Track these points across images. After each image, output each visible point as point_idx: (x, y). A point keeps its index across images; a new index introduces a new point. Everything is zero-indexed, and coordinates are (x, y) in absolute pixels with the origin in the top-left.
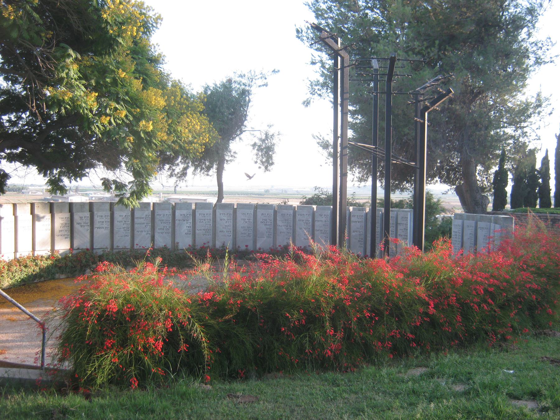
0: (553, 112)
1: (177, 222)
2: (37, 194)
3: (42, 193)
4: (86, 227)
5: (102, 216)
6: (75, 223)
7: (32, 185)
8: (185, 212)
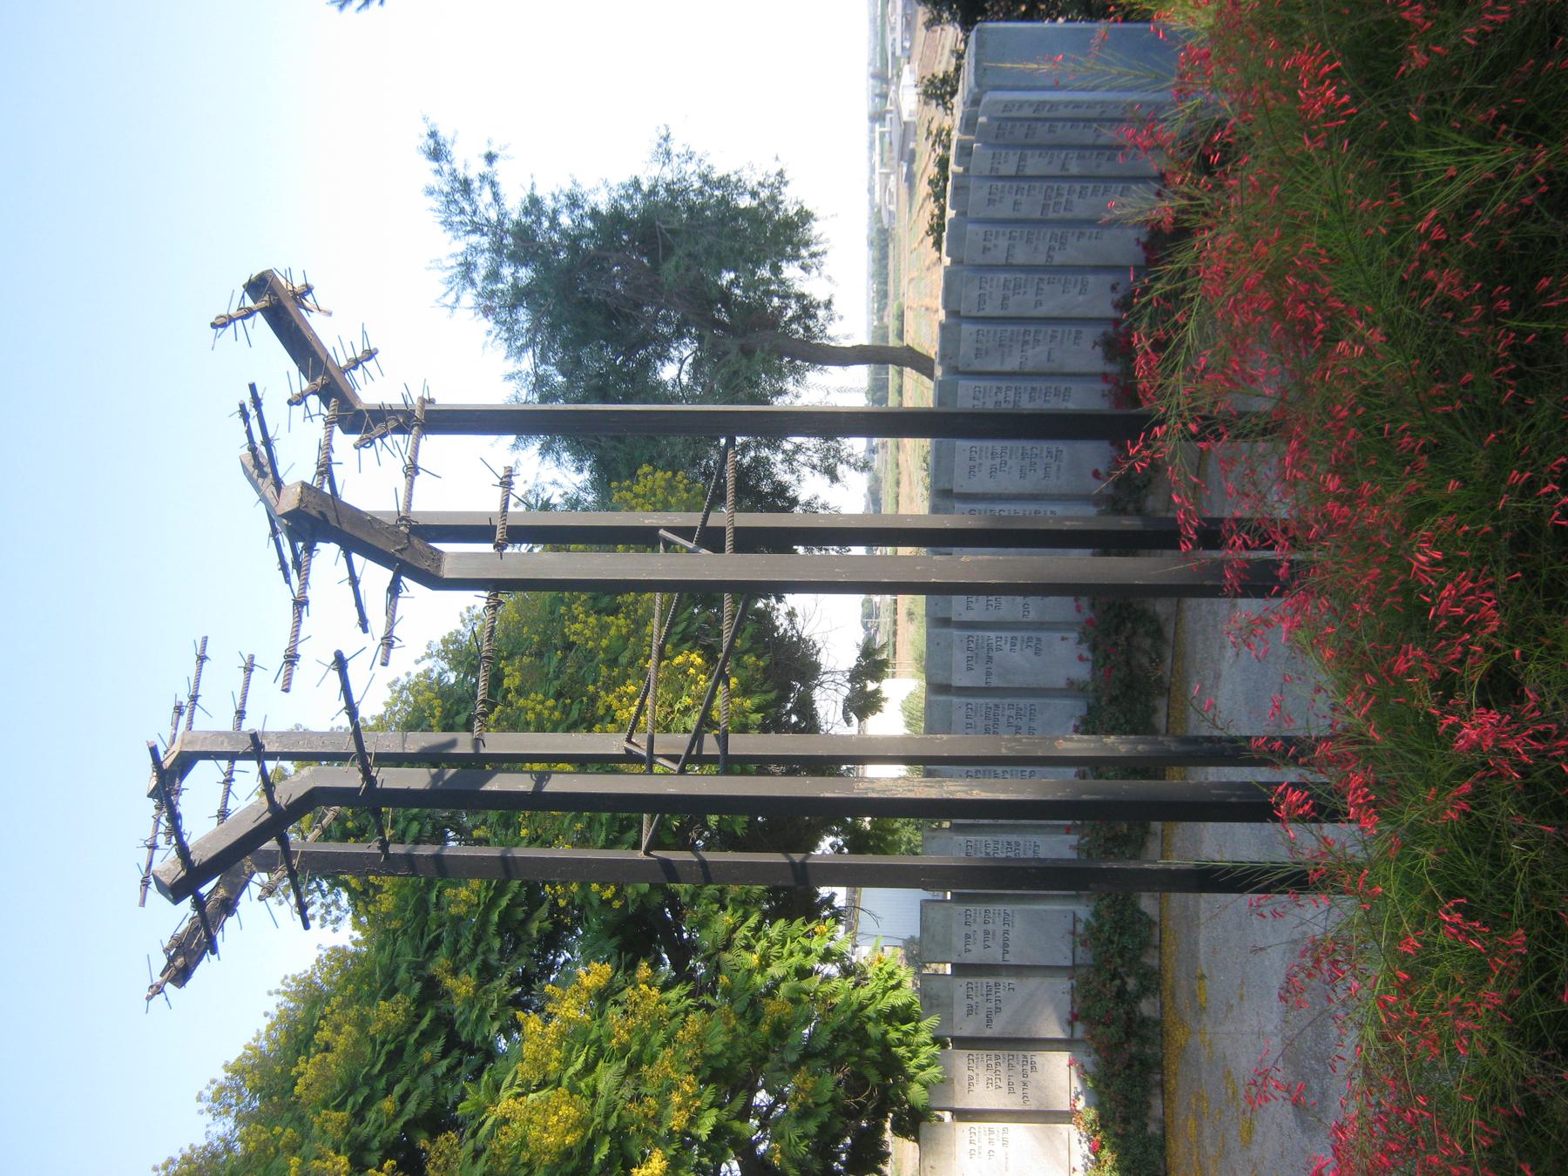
0: (300, 650)
1: (995, 682)
2: (894, 190)
3: (893, 177)
4: (1002, 993)
5: (967, 936)
6: (988, 1033)
7: (871, 190)
8: (959, 657)
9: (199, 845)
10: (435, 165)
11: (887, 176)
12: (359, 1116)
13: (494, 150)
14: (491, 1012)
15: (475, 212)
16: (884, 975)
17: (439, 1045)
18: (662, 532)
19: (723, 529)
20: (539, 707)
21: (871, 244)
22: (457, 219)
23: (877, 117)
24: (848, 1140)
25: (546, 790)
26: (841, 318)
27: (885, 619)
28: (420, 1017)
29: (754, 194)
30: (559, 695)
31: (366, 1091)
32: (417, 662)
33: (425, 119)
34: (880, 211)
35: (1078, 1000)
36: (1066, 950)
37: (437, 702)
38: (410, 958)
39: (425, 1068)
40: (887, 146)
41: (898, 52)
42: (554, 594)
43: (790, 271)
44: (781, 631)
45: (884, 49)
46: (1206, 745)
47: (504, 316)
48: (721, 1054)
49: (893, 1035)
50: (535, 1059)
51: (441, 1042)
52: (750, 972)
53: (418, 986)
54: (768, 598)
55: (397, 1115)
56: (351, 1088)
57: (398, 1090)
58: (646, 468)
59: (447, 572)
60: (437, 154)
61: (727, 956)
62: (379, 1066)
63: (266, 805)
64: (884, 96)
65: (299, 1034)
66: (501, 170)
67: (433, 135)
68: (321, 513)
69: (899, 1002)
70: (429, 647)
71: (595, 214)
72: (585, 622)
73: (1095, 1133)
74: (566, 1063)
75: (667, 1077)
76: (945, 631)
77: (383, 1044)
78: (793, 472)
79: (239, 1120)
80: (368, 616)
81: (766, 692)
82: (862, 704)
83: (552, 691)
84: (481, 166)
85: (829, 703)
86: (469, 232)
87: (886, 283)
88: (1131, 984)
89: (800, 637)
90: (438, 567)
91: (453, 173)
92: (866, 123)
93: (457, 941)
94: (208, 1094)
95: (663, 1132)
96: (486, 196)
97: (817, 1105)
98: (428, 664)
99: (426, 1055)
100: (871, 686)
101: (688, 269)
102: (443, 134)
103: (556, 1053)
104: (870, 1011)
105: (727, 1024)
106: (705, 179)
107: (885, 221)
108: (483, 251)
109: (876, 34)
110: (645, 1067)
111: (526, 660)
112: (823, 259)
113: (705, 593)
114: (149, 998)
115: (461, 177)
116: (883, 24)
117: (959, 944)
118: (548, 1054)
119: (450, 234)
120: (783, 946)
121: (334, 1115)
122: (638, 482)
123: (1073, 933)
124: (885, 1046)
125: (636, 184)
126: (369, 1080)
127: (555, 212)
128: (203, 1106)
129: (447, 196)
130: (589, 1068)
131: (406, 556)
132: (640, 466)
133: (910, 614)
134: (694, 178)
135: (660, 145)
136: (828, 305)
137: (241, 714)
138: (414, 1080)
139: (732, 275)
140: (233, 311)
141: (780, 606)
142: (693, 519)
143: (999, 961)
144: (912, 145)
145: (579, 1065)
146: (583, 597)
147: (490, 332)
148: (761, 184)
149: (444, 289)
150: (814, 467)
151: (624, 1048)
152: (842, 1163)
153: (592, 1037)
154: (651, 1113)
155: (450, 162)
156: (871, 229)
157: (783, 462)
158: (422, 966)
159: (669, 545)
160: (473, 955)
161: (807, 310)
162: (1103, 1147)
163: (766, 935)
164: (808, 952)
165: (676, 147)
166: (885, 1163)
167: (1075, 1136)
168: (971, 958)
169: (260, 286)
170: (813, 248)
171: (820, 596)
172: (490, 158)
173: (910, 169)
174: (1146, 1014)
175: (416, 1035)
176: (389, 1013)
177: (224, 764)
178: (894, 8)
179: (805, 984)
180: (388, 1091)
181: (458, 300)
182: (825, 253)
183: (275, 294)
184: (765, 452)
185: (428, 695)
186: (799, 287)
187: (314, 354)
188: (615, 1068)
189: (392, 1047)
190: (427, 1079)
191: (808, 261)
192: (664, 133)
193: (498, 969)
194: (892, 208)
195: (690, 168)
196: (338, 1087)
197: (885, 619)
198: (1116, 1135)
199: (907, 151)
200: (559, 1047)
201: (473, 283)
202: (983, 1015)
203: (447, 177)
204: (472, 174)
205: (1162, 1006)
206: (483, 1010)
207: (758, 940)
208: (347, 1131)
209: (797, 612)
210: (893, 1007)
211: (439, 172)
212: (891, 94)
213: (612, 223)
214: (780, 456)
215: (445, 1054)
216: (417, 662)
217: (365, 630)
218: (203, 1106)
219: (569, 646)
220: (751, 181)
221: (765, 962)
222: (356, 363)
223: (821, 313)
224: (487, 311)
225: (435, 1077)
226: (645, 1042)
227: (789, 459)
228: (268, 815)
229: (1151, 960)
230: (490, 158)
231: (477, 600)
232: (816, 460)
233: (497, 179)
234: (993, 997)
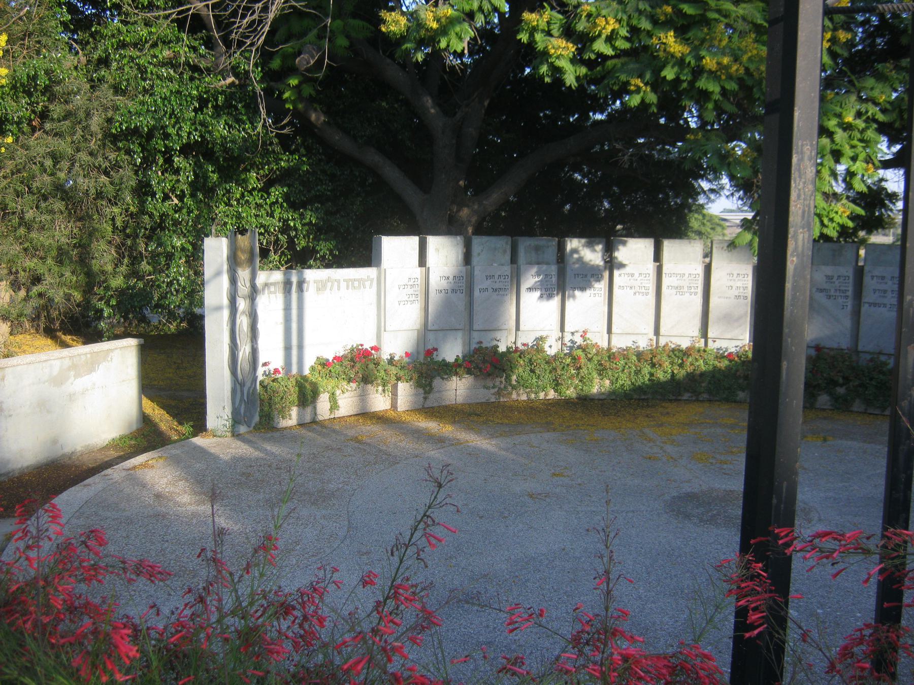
4: (840, 300)
5: (883, 278)
16: (832, 215)
35: (832, 353)
36: (870, 347)
46: (903, 476)
52: (839, 116)
61: (853, 98)
73: (740, 357)
75: (745, 52)
88: (841, 391)
92: (818, 71)
95: (703, 53)
110: (753, 36)
117: (878, 271)
123: (880, 353)
143: (864, 300)
162: (730, 361)
163: (867, 128)
167: (740, 343)
168: (867, 279)
174: (819, 398)
188: (758, 15)
198: (737, 371)
202: (826, 286)
205: (824, 410)
221: (847, 127)
229: (857, 406)
234: (838, 294)
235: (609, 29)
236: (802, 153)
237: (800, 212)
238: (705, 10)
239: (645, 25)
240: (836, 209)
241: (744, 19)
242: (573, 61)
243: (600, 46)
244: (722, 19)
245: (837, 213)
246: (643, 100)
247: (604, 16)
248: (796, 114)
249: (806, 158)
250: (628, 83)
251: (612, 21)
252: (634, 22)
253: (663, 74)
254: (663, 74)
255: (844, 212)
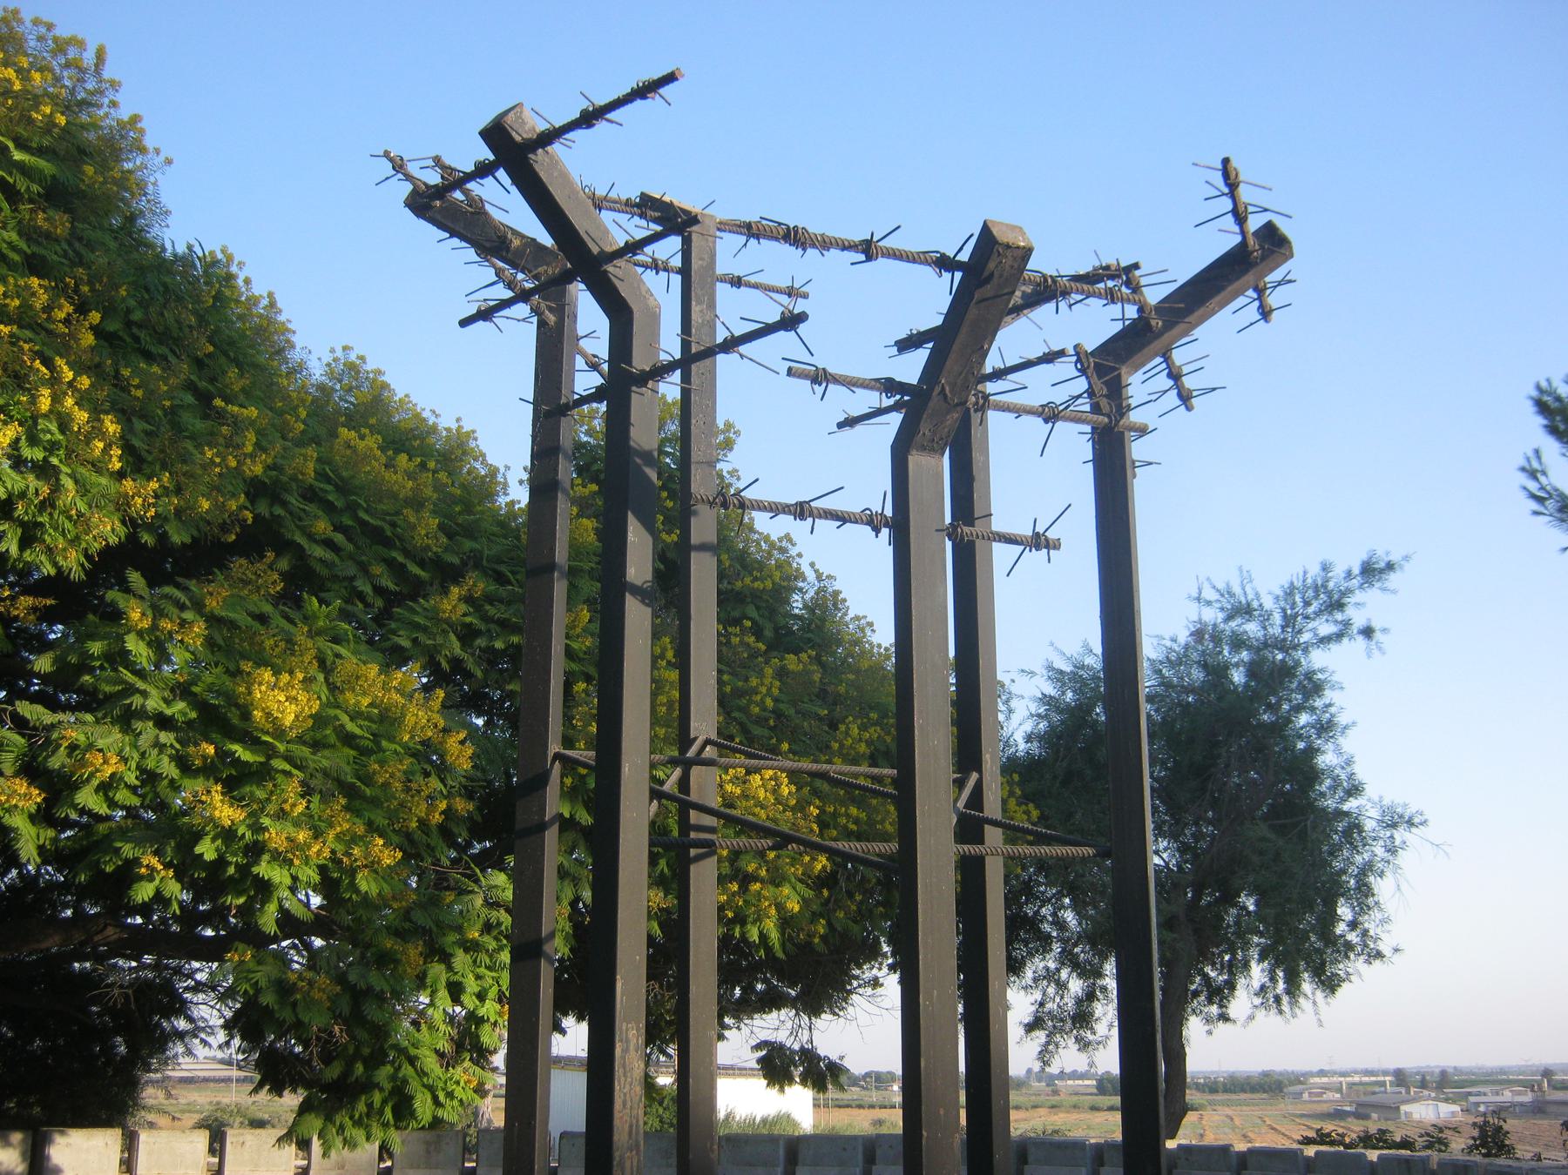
7: (1322, 1073)
9: (555, 163)
10: (1356, 571)
11: (1340, 1090)
12: (310, 495)
13: (1378, 635)
14: (422, 638)
15: (1307, 617)
17: (388, 583)
18: (975, 776)
19: (982, 843)
20: (764, 690)
21: (1266, 1074)
22: (1298, 599)
23: (1400, 1077)
24: (298, 1049)
25: (629, 598)
26: (1210, 1033)
27: (875, 1096)
28: (422, 564)
29: (1353, 925)
30: (778, 714)
31: (339, 504)
32: (812, 565)
33: (1406, 558)
34: (1301, 1083)
37: (769, 584)
38: (486, 552)
39: (364, 568)
40: (1370, 1089)
41: (1472, 1099)
42: (893, 708)
43: (1257, 973)
44: (856, 972)
45: (1473, 1083)
47: (1195, 656)
48: (357, 891)
49: (377, 1098)
50: (358, 678)
51: (392, 586)
53: (456, 560)
54: (894, 954)
55: (311, 537)
56: (343, 488)
57: (339, 538)
58: (1035, 813)
59: (916, 460)
60: (1371, 572)
62: (366, 517)
63: (609, 249)
64: (1423, 1084)
65: (408, 439)
66: (1354, 647)
67: (1390, 567)
68: (992, 275)
69: (417, 1104)
70: (829, 577)
71: (1312, 751)
72: (860, 740)
74: (355, 716)
76: (860, 1157)
77: (393, 525)
78: (1035, 980)
79: (321, 387)
80: (859, 428)
81: (783, 945)
82: (776, 1065)
83: (782, 706)
84: (1359, 621)
85: (777, 1026)
86: (1284, 610)
87: (1226, 1090)
89: (850, 992)
90: (923, 448)
91: (1349, 592)
93: (501, 601)
94: (353, 357)
95: (266, 821)
96: (1326, 629)
97: (294, 1005)
98: (810, 575)
99: (377, 569)
100: (797, 1072)
101: (1261, 853)
102: (1393, 579)
103: (366, 701)
104: (407, 1070)
105: (394, 898)
106: (1367, 868)
107: (1291, 1089)
108: (1265, 628)
109: (1492, 1074)
110: (343, 801)
111: (817, 677)
112: (1274, 1011)
113: (900, 873)
114: (387, 155)
115: (1346, 600)
116: (1501, 1082)
118: (364, 694)
119: (1280, 592)
120: (489, 968)
121: (311, 465)
122: (1019, 804)
124: (367, 1086)
125: (1354, 790)
126: (352, 508)
127: (1313, 709)
128: (339, 353)
129: (1324, 586)
130: (348, 739)
131: (935, 401)
132: (1037, 807)
133: (880, 1122)
134: (1366, 856)
135: (1401, 817)
136: (1224, 1018)
137: (737, 282)
138: (351, 557)
139: (1251, 908)
140: (1245, 193)
141: (885, 970)
142: (992, 808)
144: (1375, 1116)
145: (351, 727)
146: (888, 739)
147: (1174, 640)
148: (1365, 933)
149: (1221, 586)
150: (1042, 1004)
151: (368, 780)
152: (273, 1042)
153: (384, 743)
154: (287, 807)
155: (1361, 587)
156: (1281, 1074)
157: (1047, 969)
158: (477, 566)
159: (960, 784)
160: (486, 618)
161: (1219, 994)
164: (481, 997)
165: (1400, 835)
166: (270, 1091)
169: (1273, 244)
170: (1285, 999)
171: (898, 1014)
172: (1368, 632)
173: (1348, 1114)
175: (401, 559)
176: (426, 529)
177: (677, 262)
178: (1519, 1093)
179: (443, 993)
180: (337, 528)
181: (1209, 603)
182: (1281, 1012)
183: (1263, 258)
184: (1057, 948)
185: (777, 575)
186: (1241, 982)
187: (1189, 311)
188: (348, 769)
189: (389, 533)
190: (352, 570)
191: (1270, 996)
192: (1416, 820)
193: (471, 646)
194: (1306, 1096)
195: (1379, 851)
196: (344, 474)
197: (875, 1096)
199: (1368, 1111)
200: (371, 705)
201: (1230, 618)
203: (1344, 586)
204: (1350, 612)
206: (425, 629)
207: (496, 939)
208: (294, 479)
209: (879, 990)
210: (412, 1098)
211: (1349, 575)
212: (1426, 1093)
213: (1304, 771)
214: (1052, 965)
215: (379, 590)
216: (812, 565)
217: (841, 425)
218: (339, 353)
219: (833, 726)
220: (1370, 923)
222: (1175, 376)
223: (1214, 1009)
224: (1198, 634)
225: (352, 579)
226: (375, 802)
227: (1050, 976)
228: (595, 250)
230: (1368, 632)
231: (883, 635)
232: (1049, 1006)
233: (1345, 640)
235: (109, 771)
236: (628, 1041)
237: (627, 1127)
238: (269, 758)
239: (169, 769)
240: (456, 1077)
241: (326, 773)
242: (33, 818)
243: (88, 798)
244: (295, 772)
245: (458, 1083)
246: (158, 893)
247: (100, 750)
248: (619, 985)
249: (632, 1047)
250: (136, 862)
251: (114, 760)
252: (150, 764)
253: (198, 850)
254: (198, 850)
255: (469, 1081)
